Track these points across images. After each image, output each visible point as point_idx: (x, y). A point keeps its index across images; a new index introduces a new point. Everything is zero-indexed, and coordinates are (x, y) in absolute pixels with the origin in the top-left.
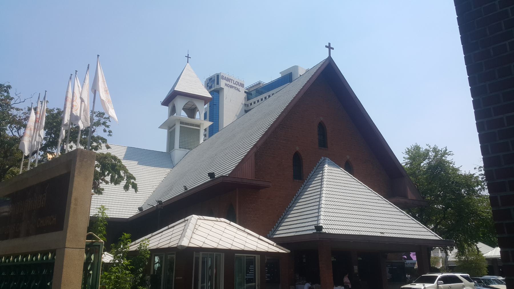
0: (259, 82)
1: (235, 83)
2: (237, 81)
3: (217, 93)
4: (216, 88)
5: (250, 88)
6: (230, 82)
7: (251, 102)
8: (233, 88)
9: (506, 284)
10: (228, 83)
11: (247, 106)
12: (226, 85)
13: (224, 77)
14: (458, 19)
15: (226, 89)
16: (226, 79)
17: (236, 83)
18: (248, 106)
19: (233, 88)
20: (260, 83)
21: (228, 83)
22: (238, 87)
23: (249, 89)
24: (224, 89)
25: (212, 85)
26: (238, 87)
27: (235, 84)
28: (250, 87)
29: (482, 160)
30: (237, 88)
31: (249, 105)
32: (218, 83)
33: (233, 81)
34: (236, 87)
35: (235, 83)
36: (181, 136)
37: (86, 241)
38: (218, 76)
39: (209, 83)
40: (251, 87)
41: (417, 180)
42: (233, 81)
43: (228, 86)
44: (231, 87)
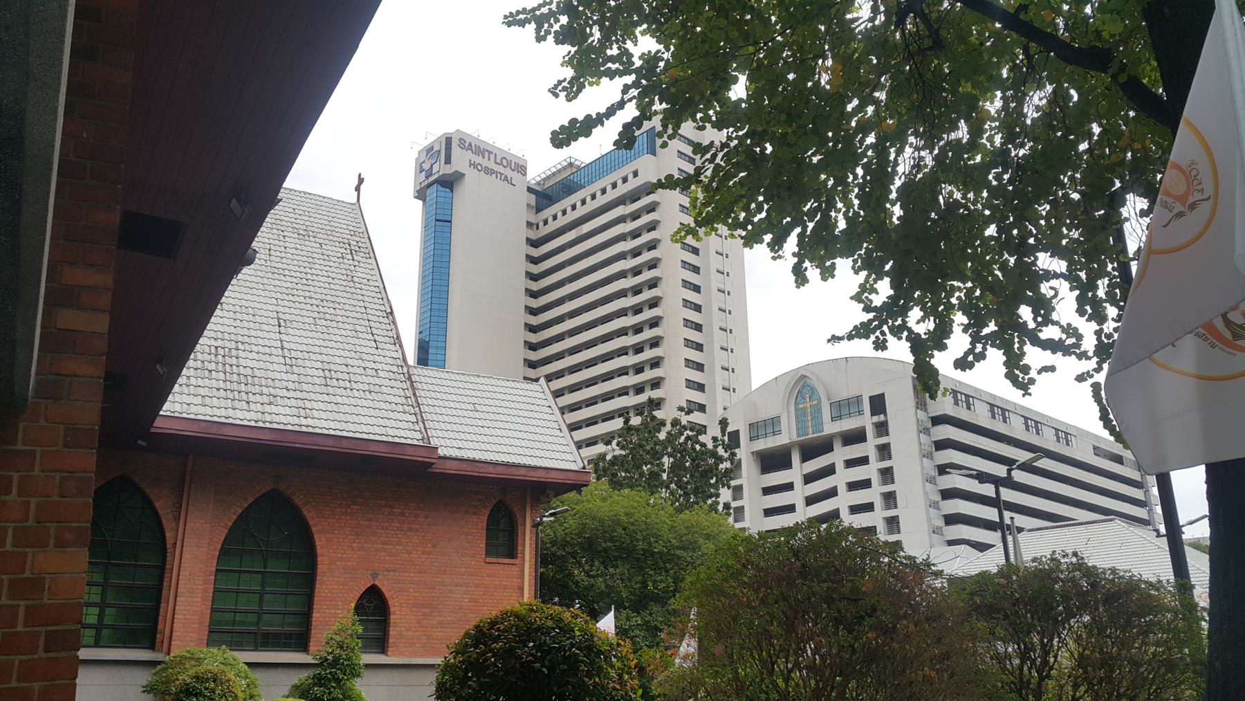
0: (568, 160)
1: (498, 161)
2: (504, 158)
3: (448, 190)
4: (443, 174)
5: (544, 180)
6: (483, 157)
7: (545, 217)
8: (494, 176)
9: (1210, 554)
10: (478, 159)
11: (535, 227)
12: (473, 165)
13: (467, 144)
14: (1208, 492)
15: (471, 176)
16: (472, 150)
17: (502, 161)
18: (538, 228)
19: (494, 176)
20: (571, 165)
21: (478, 159)
22: (508, 172)
23: (542, 182)
24: (466, 176)
25: (432, 165)
26: (508, 172)
27: (501, 164)
28: (543, 176)
29: (392, 610)
30: (506, 176)
31: (541, 224)
32: (448, 160)
33: (492, 156)
34: (501, 174)
35: (498, 161)
36: (800, 425)
37: (10, 532)
38: (448, 140)
39: (424, 162)
40: (548, 177)
41: (924, 597)
42: (492, 156)
43: (479, 168)
44: (489, 171)
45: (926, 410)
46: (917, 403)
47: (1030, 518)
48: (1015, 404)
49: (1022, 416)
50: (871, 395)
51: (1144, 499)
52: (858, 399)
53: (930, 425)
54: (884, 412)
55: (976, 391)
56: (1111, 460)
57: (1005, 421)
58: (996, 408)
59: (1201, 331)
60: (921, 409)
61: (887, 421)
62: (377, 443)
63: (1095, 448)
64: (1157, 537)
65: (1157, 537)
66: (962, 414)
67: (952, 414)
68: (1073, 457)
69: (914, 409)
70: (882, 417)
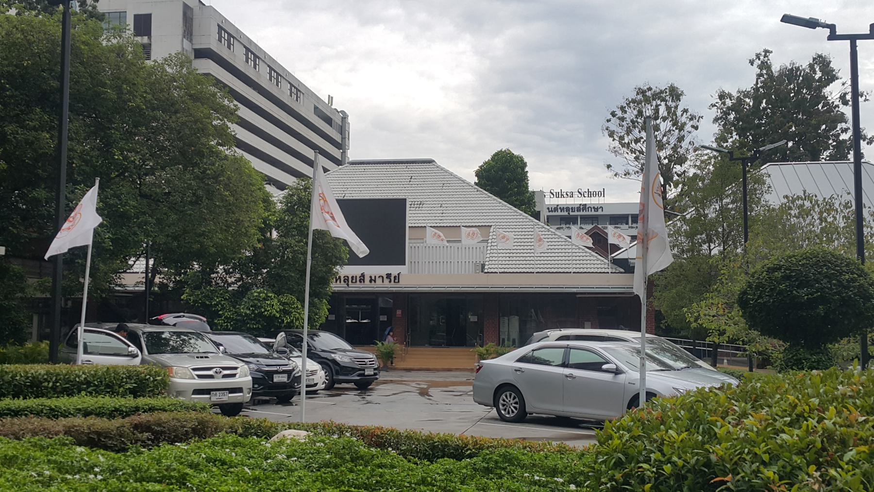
45: (191, 41)
46: (185, 31)
47: (261, 161)
48: (265, 52)
49: (269, 66)
50: (136, 13)
51: (340, 159)
52: (122, 15)
53: (192, 57)
54: (149, 34)
55: (251, 44)
56: (319, 116)
57: (229, 47)
58: (223, 32)
59: (300, 374)
60: (187, 40)
61: (150, 44)
62: (362, 167)
63: (316, 108)
64: (830, 38)
65: (830, 38)
66: (224, 53)
67: (215, 50)
68: (247, 74)
69: (181, 37)
70: (145, 40)
